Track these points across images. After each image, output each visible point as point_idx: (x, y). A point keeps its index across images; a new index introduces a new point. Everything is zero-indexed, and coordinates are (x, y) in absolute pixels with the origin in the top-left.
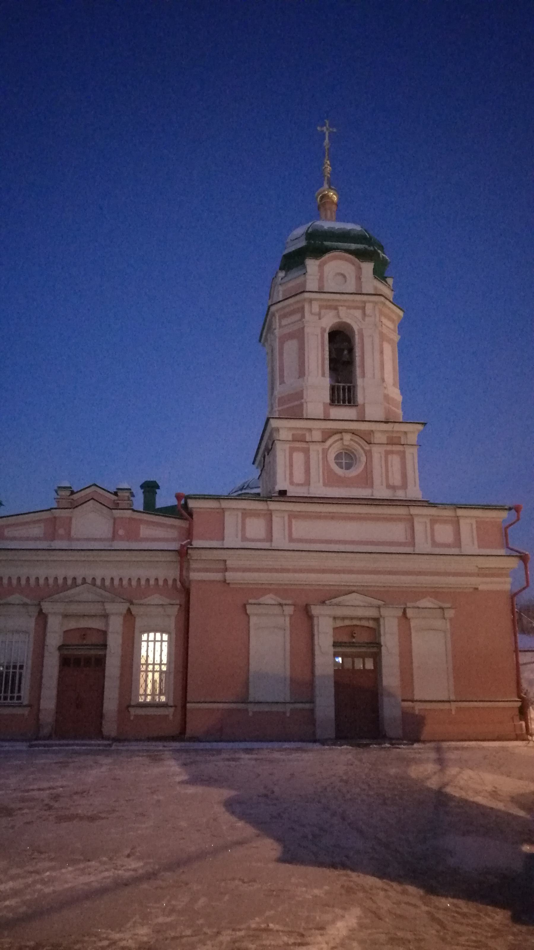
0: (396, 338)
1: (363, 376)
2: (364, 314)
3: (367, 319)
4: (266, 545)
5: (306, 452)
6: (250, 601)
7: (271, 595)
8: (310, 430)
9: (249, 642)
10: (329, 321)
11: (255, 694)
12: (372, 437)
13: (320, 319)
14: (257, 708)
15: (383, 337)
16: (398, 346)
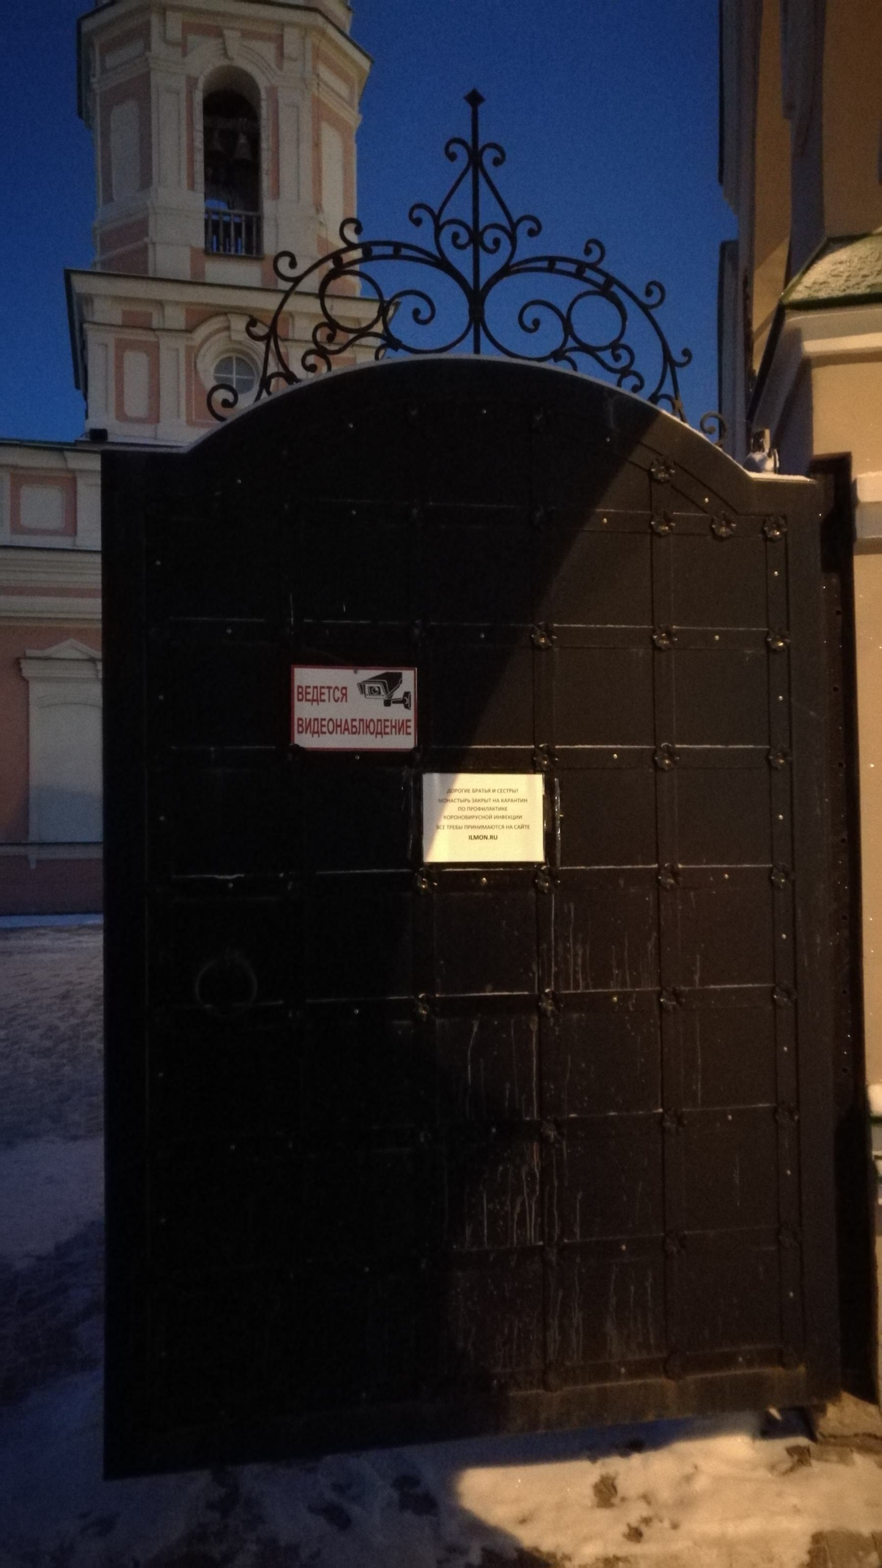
0: (353, 118)
1: (276, 195)
2: (281, 54)
3: (287, 65)
4: (64, 542)
5: (153, 352)
6: (30, 653)
7: (71, 641)
8: (160, 304)
9: (28, 733)
10: (204, 62)
11: (41, 827)
12: (290, 327)
13: (185, 54)
14: (47, 854)
15: (320, 113)
16: (357, 141)
